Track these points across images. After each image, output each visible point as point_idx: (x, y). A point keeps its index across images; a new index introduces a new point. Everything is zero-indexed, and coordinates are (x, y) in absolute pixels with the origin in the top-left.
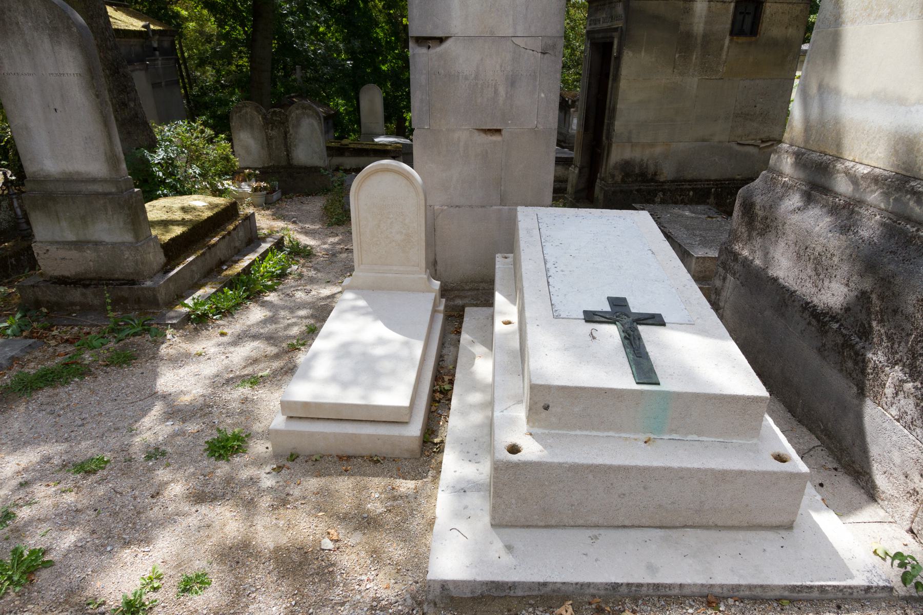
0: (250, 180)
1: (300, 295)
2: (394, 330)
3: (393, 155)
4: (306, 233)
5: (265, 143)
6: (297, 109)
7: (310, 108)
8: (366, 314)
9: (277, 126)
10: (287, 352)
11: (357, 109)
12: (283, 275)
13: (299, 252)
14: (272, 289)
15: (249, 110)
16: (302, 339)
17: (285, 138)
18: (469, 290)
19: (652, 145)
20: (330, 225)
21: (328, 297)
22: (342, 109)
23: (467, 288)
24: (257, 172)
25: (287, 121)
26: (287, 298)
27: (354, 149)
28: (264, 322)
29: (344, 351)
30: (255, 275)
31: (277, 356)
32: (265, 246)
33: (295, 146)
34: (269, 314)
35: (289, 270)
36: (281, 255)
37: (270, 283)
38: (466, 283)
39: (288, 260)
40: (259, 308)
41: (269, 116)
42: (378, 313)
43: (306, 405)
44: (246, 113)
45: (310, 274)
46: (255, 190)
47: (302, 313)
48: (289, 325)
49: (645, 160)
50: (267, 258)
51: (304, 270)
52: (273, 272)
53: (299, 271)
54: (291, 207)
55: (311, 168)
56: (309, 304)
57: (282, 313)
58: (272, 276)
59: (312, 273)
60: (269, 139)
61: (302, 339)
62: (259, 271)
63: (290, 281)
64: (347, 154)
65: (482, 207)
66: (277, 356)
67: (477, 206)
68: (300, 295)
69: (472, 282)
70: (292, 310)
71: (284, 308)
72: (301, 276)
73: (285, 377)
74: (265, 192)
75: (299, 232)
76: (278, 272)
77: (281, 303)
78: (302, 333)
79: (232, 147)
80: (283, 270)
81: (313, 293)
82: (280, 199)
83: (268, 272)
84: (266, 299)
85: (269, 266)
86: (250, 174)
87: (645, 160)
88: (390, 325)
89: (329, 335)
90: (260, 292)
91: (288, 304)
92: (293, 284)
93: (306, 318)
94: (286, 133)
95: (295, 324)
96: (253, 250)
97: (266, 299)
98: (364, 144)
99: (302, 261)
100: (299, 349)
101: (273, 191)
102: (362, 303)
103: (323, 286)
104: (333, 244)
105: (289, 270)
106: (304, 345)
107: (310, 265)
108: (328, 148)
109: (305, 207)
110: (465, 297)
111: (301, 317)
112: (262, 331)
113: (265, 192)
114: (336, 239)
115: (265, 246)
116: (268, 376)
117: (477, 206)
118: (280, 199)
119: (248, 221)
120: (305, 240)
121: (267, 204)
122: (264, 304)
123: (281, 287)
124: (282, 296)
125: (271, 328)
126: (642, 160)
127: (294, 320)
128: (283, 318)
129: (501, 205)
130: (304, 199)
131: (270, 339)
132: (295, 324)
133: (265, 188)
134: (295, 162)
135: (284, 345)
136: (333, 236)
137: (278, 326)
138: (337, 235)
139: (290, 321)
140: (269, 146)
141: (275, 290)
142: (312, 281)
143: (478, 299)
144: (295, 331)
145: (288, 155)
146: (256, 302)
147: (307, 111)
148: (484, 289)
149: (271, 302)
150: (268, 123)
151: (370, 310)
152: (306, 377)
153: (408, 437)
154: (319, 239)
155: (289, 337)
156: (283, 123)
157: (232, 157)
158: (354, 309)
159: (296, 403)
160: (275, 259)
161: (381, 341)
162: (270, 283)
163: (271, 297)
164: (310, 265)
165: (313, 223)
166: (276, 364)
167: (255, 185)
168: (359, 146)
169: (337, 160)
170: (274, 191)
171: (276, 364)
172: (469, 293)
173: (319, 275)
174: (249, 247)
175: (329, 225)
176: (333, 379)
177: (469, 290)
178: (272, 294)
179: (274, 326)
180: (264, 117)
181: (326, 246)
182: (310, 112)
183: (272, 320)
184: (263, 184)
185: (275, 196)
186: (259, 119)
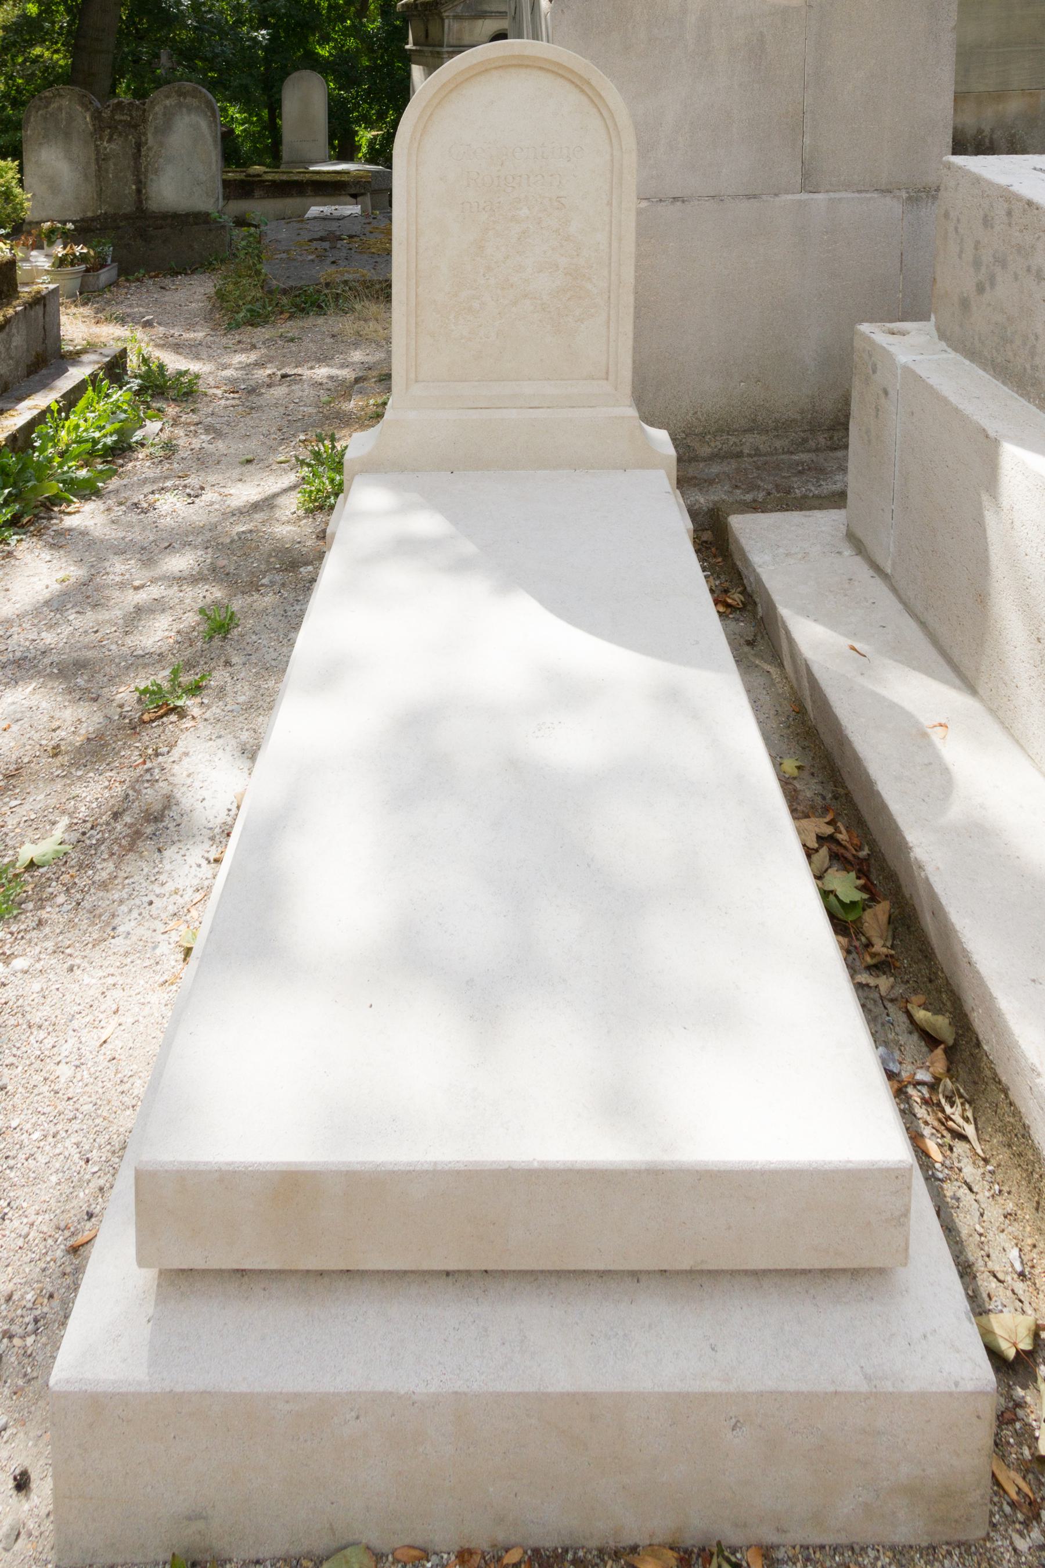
0: (51, 243)
1: (171, 506)
2: (593, 629)
3: (353, 191)
4: (177, 347)
5: (93, 167)
6: (167, 97)
7: (194, 94)
8: (461, 566)
9: (123, 136)
10: (136, 727)
11: (273, 128)
12: (120, 450)
13: (157, 387)
14: (88, 491)
15: (65, 102)
16: (189, 665)
17: (137, 155)
18: (713, 457)
19: (999, 96)
20: (233, 326)
21: (256, 507)
22: (239, 130)
23: (705, 451)
24: (70, 226)
25: (145, 121)
26: (133, 517)
27: (273, 182)
28: (58, 605)
29: (420, 759)
30: (42, 449)
31: (94, 751)
32: (75, 375)
33: (156, 172)
34: (75, 572)
35: (138, 436)
36: (119, 395)
37: (83, 473)
38: (703, 435)
39: (135, 408)
40: (46, 555)
41: (106, 114)
42: (514, 566)
43: (290, 1191)
44: (60, 109)
45: (196, 443)
46: (61, 262)
47: (180, 563)
48: (139, 611)
49: (987, 131)
50: (82, 403)
51: (180, 432)
52: (95, 442)
53: (165, 436)
54: (139, 299)
55: (187, 215)
56: (199, 531)
57: (118, 568)
58: (92, 453)
59: (201, 441)
60: (101, 159)
61: (189, 665)
62: (53, 439)
63: (140, 465)
64: (257, 194)
65: (749, 197)
66: (94, 751)
67: (735, 197)
68: (171, 506)
69: (720, 431)
70: (146, 555)
71: (120, 551)
72: (170, 448)
73: (132, 865)
74: (83, 267)
75: (157, 346)
76: (109, 441)
77: (113, 534)
78: (186, 638)
79: (21, 170)
80: (123, 434)
81: (209, 496)
82: (114, 284)
83: (79, 441)
84: (69, 522)
85: (90, 422)
86: (52, 231)
87: (987, 131)
88: (565, 604)
89: (331, 675)
90: (55, 501)
91: (136, 535)
92: (150, 473)
93: (195, 579)
94: (139, 146)
95: (158, 606)
96: (44, 385)
97: (69, 522)
98: (296, 174)
99: (172, 410)
100: (181, 712)
101: (94, 266)
102: (427, 523)
103: (236, 473)
104: (247, 367)
105: (138, 436)
106: (196, 689)
107: (195, 418)
108: (226, 183)
109: (168, 297)
110: (711, 482)
111: (179, 580)
112: (49, 638)
113: (83, 267)
114: (253, 357)
115: (75, 375)
116: (61, 859)
117: (735, 197)
118: (114, 284)
119: (39, 309)
120: (174, 363)
121: (86, 293)
122: (61, 541)
123: (114, 483)
124: (119, 511)
125: (79, 623)
126: (980, 131)
127: (155, 591)
128: (122, 586)
129: (803, 189)
130: (167, 281)
131: (76, 673)
132: (158, 606)
133: (83, 258)
134: (153, 206)
135: (125, 694)
136: (243, 351)
137: (104, 615)
138: (254, 347)
139: (142, 597)
140: (100, 174)
141: (97, 493)
142: (202, 461)
143: (752, 487)
144: (158, 633)
145: (139, 191)
146: (39, 534)
147: (189, 100)
148: (757, 453)
149: (84, 533)
150: (103, 127)
151: (469, 548)
152: (252, 936)
153: (922, 1399)
154: (211, 358)
155: (141, 660)
156: (135, 127)
157: (17, 190)
158: (407, 547)
159: (228, 1180)
160: (101, 406)
161: (568, 693)
162: (83, 473)
163: (85, 517)
164: (195, 418)
165: (190, 327)
166: (95, 791)
167: (59, 251)
168: (284, 177)
169: (239, 206)
170: (103, 266)
171: (95, 791)
172: (715, 469)
173: (220, 445)
174: (36, 378)
175: (229, 329)
176: (410, 956)
177: (713, 457)
178: (89, 507)
179: (90, 617)
180: (97, 116)
181: (228, 373)
182: (195, 102)
183: (84, 595)
184: (79, 250)
185: (105, 275)
186: (84, 120)
